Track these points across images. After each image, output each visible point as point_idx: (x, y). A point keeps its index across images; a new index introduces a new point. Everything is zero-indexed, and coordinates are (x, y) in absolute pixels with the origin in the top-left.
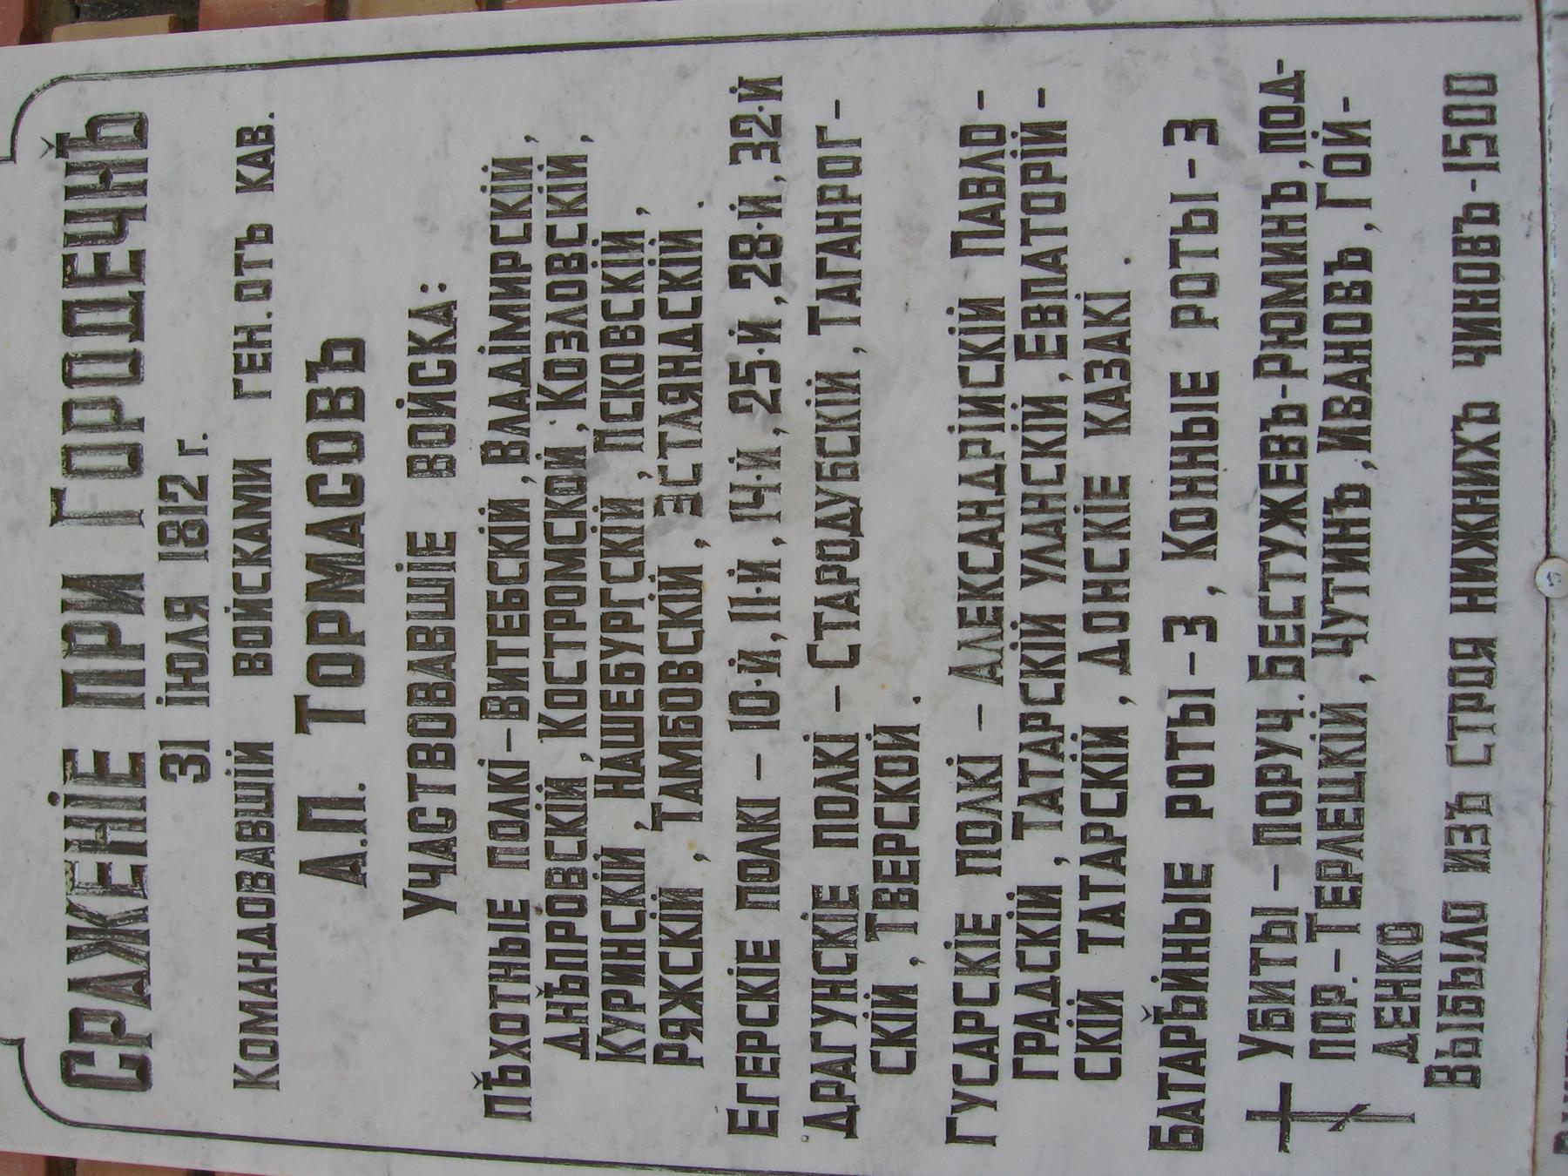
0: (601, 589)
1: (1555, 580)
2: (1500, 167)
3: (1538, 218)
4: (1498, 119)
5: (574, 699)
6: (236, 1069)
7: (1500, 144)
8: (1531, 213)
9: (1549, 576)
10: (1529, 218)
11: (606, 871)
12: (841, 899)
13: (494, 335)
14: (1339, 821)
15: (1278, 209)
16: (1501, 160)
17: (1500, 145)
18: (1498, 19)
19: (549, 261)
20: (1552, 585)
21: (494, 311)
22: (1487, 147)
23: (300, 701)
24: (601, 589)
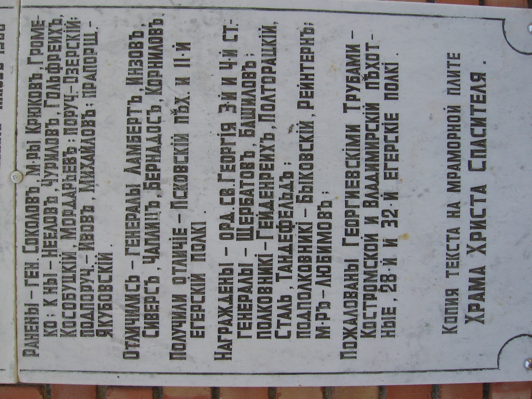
0: (275, 331)
1: (15, 178)
2: (5, 52)
3: (15, 68)
4: (5, 38)
5: (307, 268)
6: (443, 327)
7: (5, 46)
8: (13, 66)
9: (13, 177)
10: (12, 68)
11: (301, 130)
12: (222, 291)
13: (347, 145)
14: (153, 178)
15: (306, 36)
16: (6, 50)
17: (5, 46)
18: (7, 8)
19: (100, 287)
20: (14, 179)
21: (347, 137)
22: (1, 46)
23: (345, 105)
24: (275, 331)
